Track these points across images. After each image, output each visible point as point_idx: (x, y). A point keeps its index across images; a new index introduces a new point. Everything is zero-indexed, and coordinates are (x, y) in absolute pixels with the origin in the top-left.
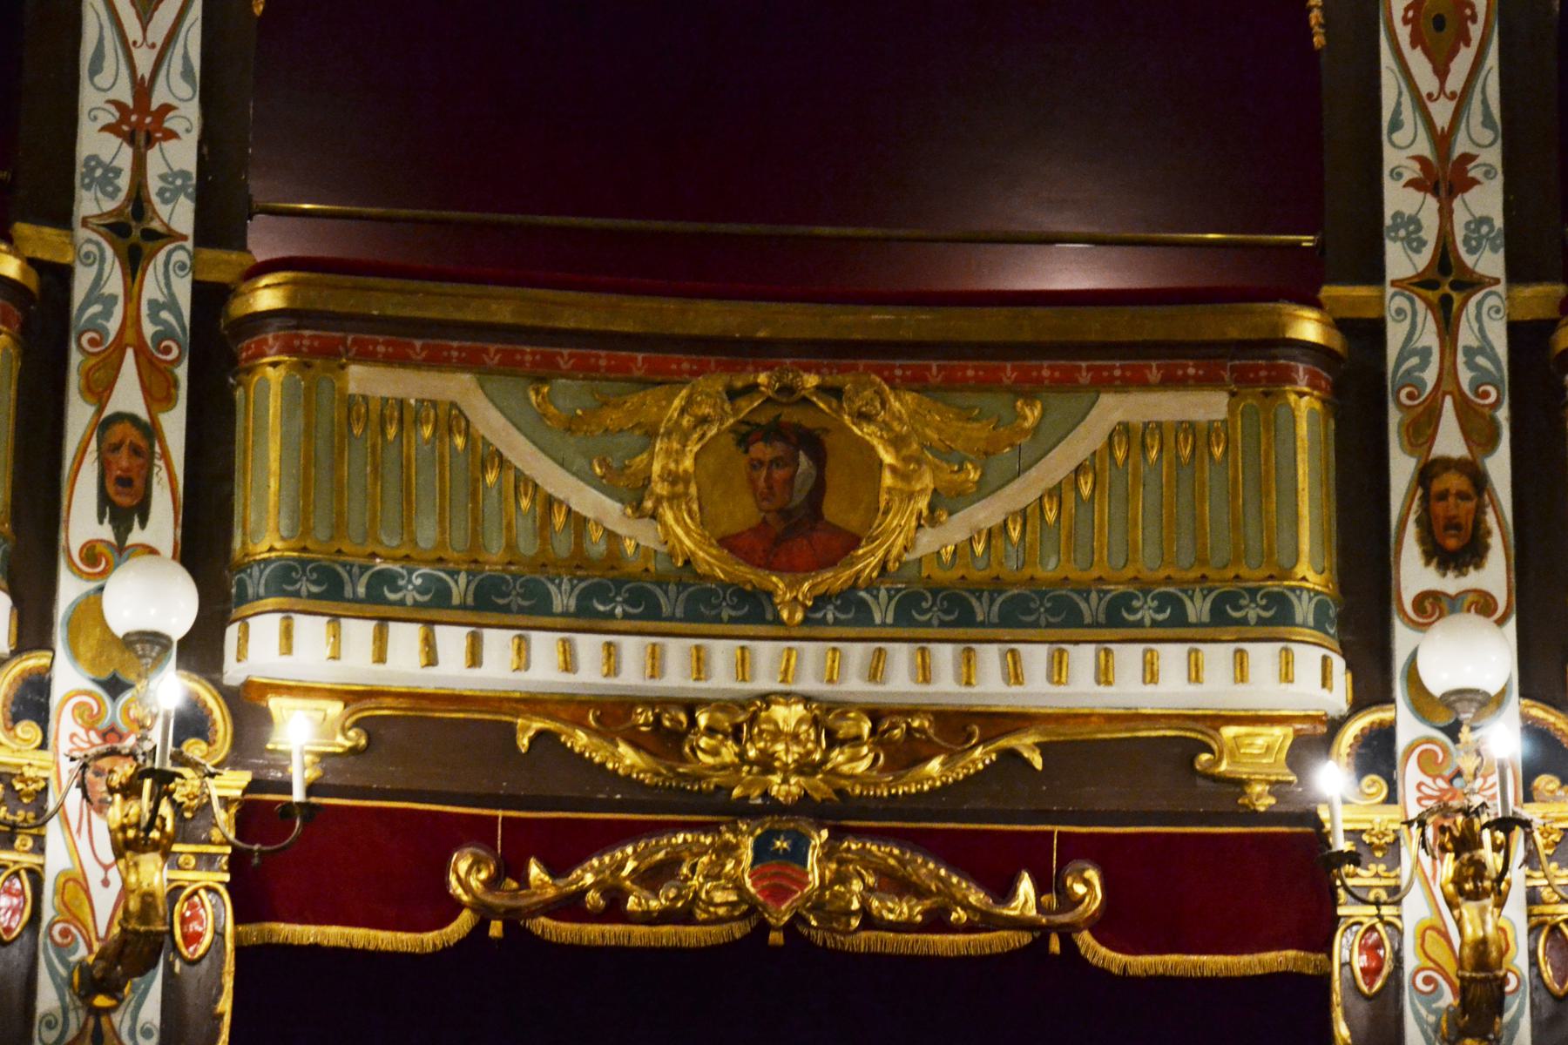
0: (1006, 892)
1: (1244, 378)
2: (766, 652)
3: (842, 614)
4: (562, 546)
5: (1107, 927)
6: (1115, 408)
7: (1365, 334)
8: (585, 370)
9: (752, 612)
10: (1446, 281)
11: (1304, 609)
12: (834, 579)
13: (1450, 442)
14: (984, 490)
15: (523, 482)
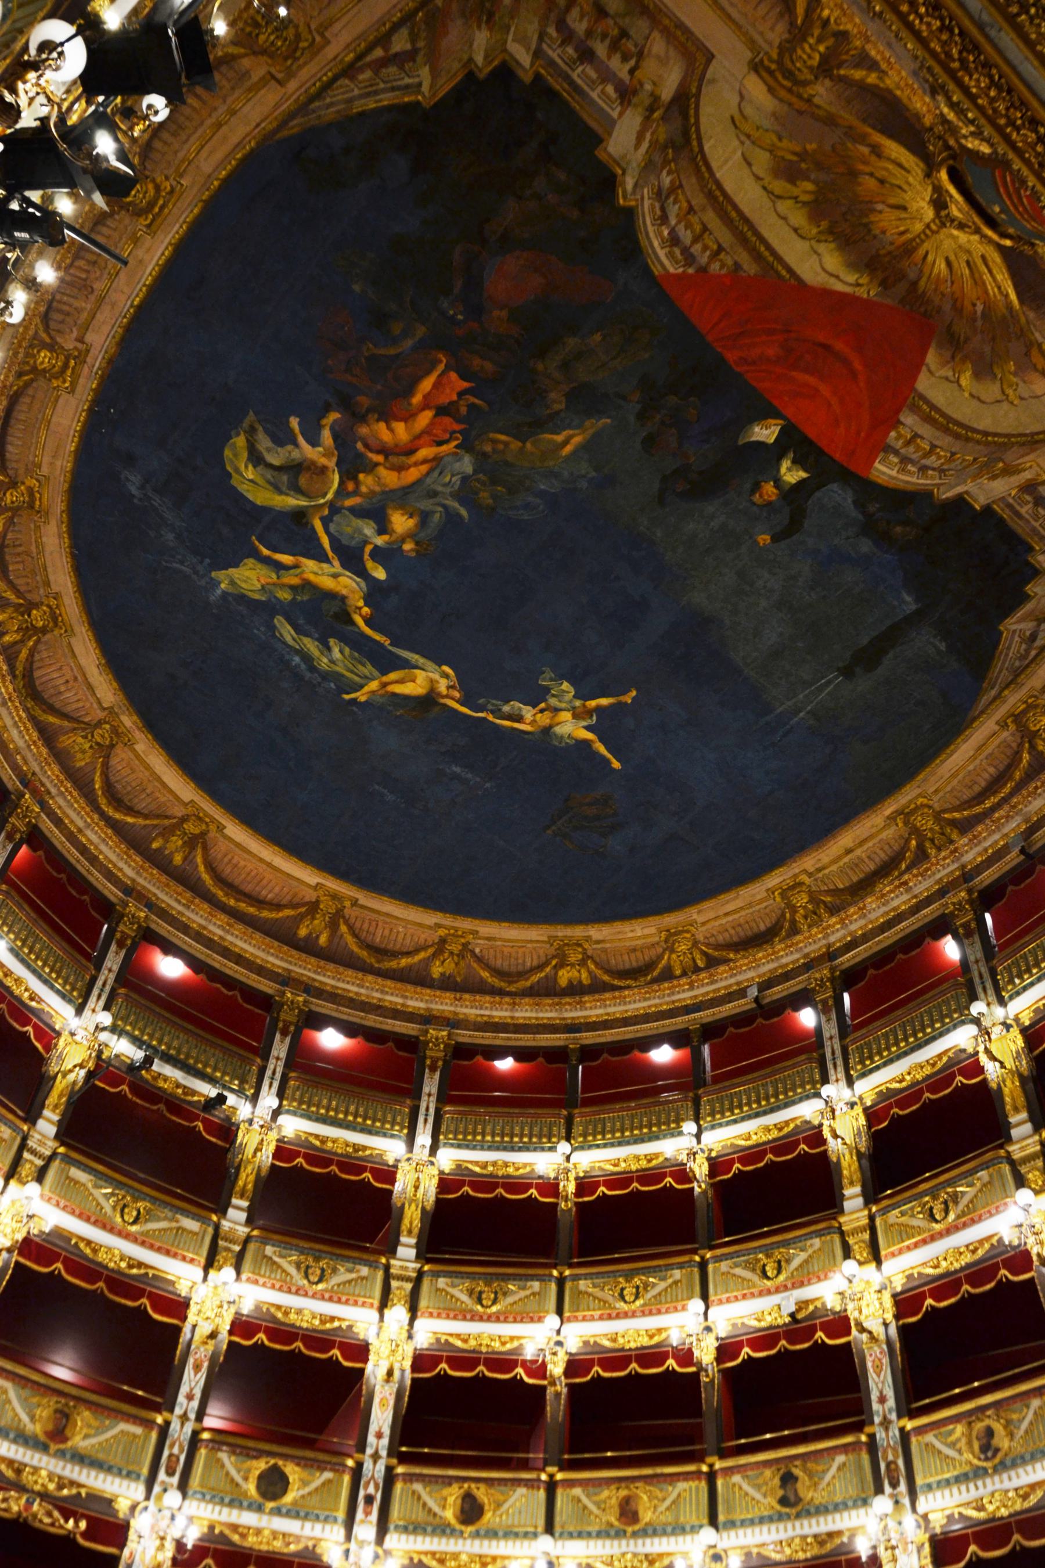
0: (67, 1521)
1: (146, 1426)
2: (45, 1458)
3: (61, 1454)
4: (15, 1424)
5: (85, 1535)
6: (123, 1426)
7: (168, 1423)
8: (32, 1388)
9: (44, 1448)
10: (376, 1457)
11: (142, 1478)
12: (62, 1446)
13: (176, 1450)
14: (95, 1435)
15: (13, 1410)
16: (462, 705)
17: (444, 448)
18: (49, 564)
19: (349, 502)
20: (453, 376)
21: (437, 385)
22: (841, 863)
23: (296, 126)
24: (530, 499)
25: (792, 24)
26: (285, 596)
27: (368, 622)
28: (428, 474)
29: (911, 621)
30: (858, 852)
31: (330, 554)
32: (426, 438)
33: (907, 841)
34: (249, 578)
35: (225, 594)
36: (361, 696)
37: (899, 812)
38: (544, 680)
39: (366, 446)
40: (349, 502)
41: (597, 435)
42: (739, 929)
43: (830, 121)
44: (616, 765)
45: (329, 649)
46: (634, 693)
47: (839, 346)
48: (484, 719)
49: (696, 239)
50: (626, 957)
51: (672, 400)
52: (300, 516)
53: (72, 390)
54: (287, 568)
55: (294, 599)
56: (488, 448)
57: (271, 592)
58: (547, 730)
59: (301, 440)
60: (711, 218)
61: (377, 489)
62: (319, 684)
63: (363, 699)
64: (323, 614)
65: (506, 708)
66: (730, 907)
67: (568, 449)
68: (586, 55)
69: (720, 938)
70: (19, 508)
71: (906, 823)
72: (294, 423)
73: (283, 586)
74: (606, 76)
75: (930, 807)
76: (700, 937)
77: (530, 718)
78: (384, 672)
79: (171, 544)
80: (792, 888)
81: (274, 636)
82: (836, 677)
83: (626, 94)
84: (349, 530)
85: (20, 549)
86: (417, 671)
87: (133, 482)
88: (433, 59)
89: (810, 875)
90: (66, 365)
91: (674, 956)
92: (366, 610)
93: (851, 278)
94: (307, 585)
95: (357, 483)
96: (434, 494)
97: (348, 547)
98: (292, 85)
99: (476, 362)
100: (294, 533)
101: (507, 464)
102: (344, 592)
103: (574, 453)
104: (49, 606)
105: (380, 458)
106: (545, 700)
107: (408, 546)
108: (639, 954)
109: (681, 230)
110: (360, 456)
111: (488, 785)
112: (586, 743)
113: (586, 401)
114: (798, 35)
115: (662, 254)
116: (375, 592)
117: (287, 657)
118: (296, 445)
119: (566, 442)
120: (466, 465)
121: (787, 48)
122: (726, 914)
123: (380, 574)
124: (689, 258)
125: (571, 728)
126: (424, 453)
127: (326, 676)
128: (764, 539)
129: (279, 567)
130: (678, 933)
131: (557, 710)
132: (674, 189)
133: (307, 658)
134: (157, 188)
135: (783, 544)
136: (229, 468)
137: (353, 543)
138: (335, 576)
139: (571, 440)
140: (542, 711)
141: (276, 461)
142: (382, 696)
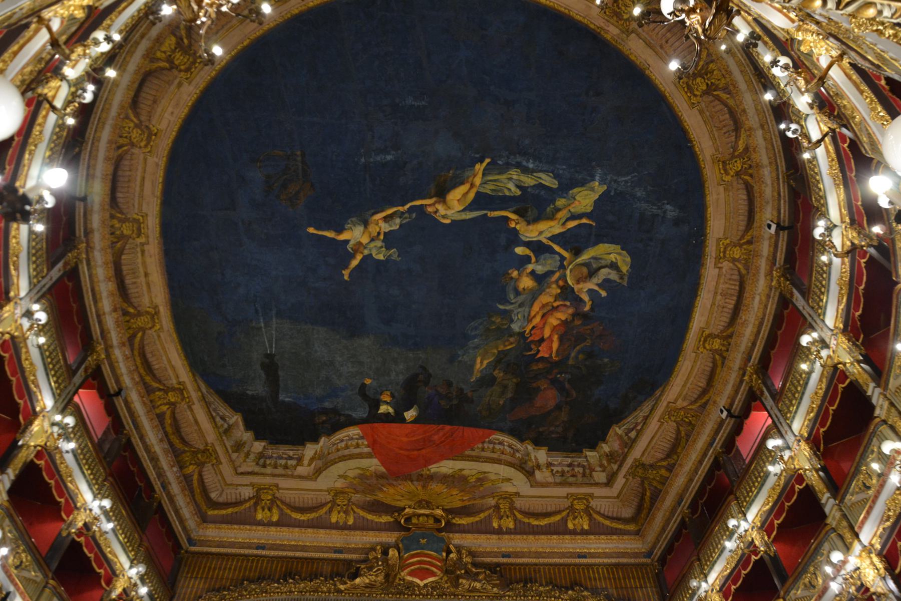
16: (422, 205)
17: (530, 327)
18: (703, 126)
19: (557, 275)
20: (547, 356)
21: (551, 348)
22: (140, 265)
23: (658, 393)
24: (477, 332)
25: (516, 509)
26: (560, 202)
27: (507, 219)
28: (530, 312)
29: (275, 393)
30: (142, 279)
31: (550, 243)
32: (541, 326)
33: (135, 308)
34: (585, 199)
35: (593, 180)
36: (480, 168)
37: (157, 313)
38: (394, 253)
39: (565, 306)
40: (557, 275)
41: (472, 374)
42: (126, 179)
43: (483, 497)
44: (311, 230)
45: (517, 186)
46: (346, 278)
47: (416, 453)
48: (403, 205)
49: (494, 448)
50: (153, 93)
51: (455, 402)
52: (577, 252)
53: (719, 240)
54: (568, 220)
55: (554, 204)
56: (512, 339)
57: (569, 199)
58: (366, 224)
59: (596, 288)
60: (495, 456)
61: (548, 290)
62: (508, 158)
63: (477, 166)
64: (535, 205)
65: (398, 221)
66: (148, 184)
67: (479, 360)
68: (570, 465)
69: (126, 163)
70: (731, 159)
71: (147, 313)
72: (604, 294)
73: (565, 207)
74: (560, 465)
75: (151, 328)
76: (135, 151)
77: (380, 223)
78: (478, 194)
79: (637, 189)
80: (139, 229)
81: (552, 172)
82: (271, 351)
83: (549, 465)
84: (549, 262)
85: (725, 130)
86: (461, 208)
87: (671, 211)
88: (620, 437)
89: (142, 244)
90: (724, 252)
91: (132, 125)
92: (513, 225)
93: (432, 471)
94: (551, 217)
95: (559, 286)
96: (521, 305)
97: (543, 253)
98: (665, 404)
99: (541, 366)
100: (575, 242)
101: (498, 339)
102: (531, 227)
103: (475, 361)
104: (695, 96)
105: (555, 304)
106: (383, 241)
107: (515, 274)
108: (149, 103)
109: (502, 447)
110: (565, 300)
111: (363, 160)
112: (340, 231)
113: (487, 381)
114: (512, 508)
115: (501, 438)
116: (514, 238)
117: (537, 163)
118: (598, 285)
119: (482, 362)
120: (516, 327)
121: (512, 503)
122: (143, 179)
123: (519, 250)
124: (490, 442)
125: (354, 234)
126: (538, 319)
127: (507, 167)
128: (368, 382)
129: (573, 217)
130: (149, 139)
131: (372, 240)
132: (513, 455)
133: (525, 171)
134: (705, 348)
135: (359, 385)
136: (624, 252)
137: (542, 257)
138: (541, 233)
139: (480, 364)
140: (379, 234)
141: (603, 271)
142: (468, 177)
